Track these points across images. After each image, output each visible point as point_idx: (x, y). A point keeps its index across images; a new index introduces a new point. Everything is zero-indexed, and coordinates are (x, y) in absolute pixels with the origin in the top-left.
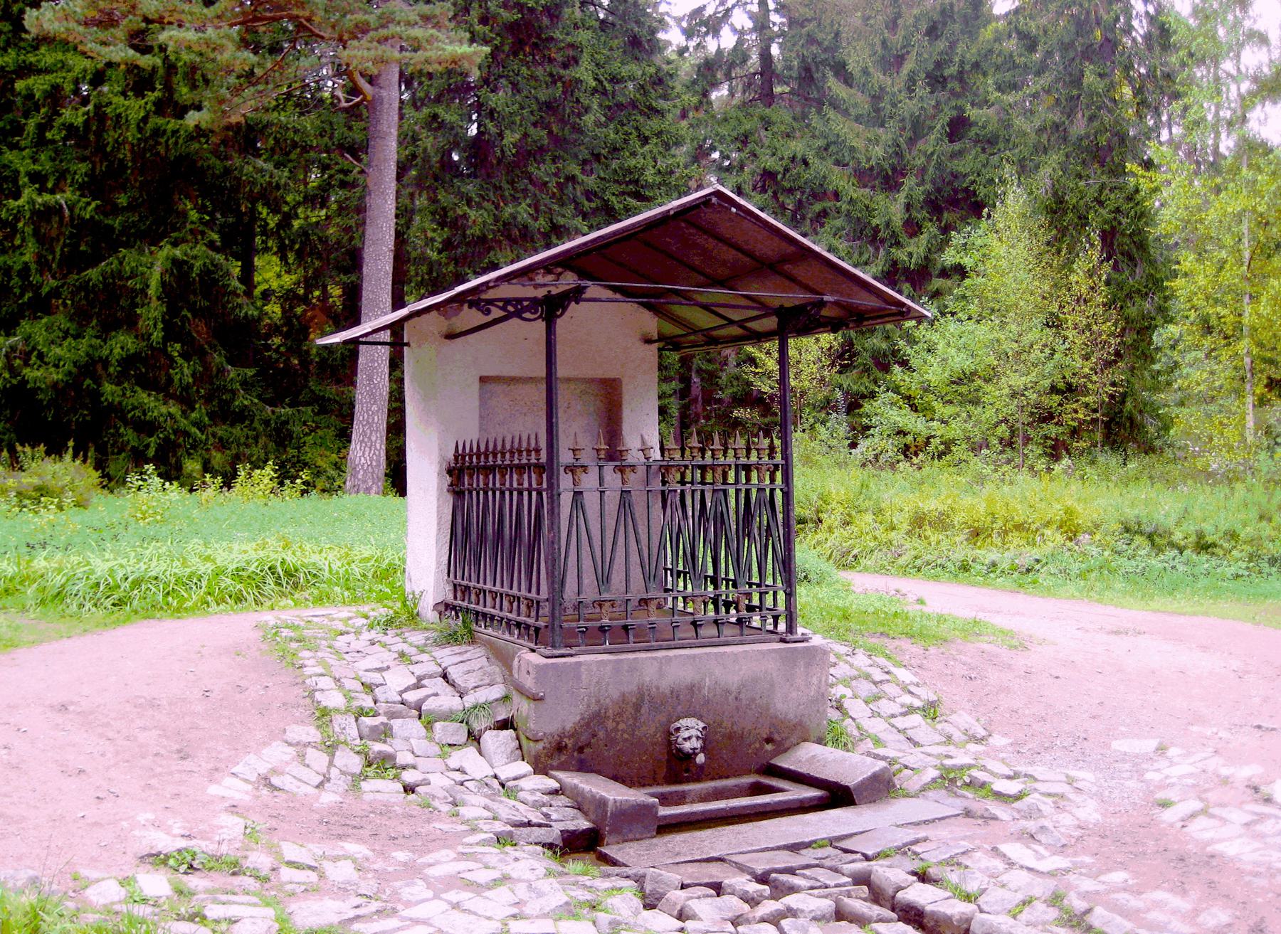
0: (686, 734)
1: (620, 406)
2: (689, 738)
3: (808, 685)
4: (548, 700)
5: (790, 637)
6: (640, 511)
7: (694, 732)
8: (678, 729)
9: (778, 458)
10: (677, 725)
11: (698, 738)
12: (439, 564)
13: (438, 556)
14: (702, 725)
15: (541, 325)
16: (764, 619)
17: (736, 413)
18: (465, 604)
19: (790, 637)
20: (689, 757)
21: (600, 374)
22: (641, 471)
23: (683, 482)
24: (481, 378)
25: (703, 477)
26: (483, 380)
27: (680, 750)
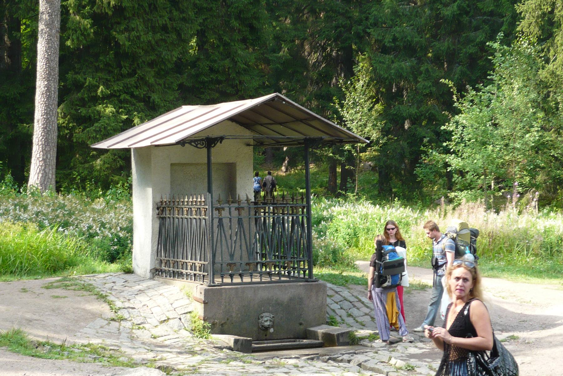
0: (266, 319)
1: (235, 174)
2: (267, 321)
5: (309, 280)
6: (246, 225)
8: (262, 317)
9: (305, 203)
10: (262, 315)
12: (152, 251)
13: (152, 247)
15: (205, 150)
16: (299, 272)
17: (487, 44)
18: (167, 269)
19: (309, 280)
20: (267, 329)
21: (225, 161)
22: (246, 209)
23: (283, 214)
24: (172, 165)
25: (293, 212)
26: (172, 165)
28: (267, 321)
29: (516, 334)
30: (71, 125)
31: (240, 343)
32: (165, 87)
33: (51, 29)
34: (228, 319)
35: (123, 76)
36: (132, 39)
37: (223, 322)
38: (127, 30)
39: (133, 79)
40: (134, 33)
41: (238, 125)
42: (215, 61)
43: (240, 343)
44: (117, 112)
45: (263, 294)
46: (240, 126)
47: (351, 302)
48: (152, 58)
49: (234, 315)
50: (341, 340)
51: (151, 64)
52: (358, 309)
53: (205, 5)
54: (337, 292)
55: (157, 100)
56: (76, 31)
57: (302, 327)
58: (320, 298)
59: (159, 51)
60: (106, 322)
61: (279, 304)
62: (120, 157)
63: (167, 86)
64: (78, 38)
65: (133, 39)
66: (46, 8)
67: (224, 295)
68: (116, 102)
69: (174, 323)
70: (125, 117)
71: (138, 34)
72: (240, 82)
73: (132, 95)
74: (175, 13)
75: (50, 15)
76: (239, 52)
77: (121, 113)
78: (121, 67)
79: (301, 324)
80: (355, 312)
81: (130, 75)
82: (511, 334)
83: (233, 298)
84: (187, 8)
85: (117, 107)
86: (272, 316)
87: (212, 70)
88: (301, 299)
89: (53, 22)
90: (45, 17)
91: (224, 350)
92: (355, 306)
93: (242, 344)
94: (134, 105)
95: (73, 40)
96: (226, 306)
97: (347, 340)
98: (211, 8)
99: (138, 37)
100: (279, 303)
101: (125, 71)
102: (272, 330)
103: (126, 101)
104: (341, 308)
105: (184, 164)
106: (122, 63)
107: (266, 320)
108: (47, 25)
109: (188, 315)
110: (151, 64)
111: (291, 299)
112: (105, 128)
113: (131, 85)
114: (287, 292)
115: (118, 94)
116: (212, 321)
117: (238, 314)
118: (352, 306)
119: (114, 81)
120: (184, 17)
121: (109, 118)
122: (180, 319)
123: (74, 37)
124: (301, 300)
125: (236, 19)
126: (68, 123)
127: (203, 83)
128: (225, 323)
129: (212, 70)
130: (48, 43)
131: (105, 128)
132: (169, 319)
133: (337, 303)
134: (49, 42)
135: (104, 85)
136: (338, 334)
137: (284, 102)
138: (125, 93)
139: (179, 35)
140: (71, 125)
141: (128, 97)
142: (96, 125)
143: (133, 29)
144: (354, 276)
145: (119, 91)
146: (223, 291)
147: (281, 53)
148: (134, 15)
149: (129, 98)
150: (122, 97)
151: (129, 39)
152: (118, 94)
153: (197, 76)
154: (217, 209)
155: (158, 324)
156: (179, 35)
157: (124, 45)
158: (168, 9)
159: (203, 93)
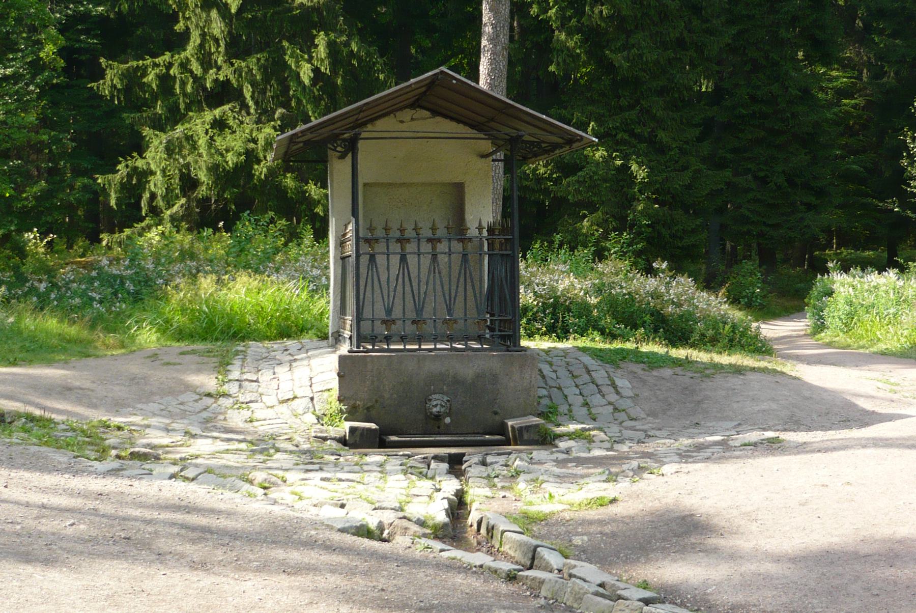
0: (435, 403)
2: (436, 405)
7: (439, 402)
8: (430, 400)
11: (442, 406)
20: (438, 417)
27: (431, 413)
28: (436, 405)
29: (783, 436)
30: (555, 176)
31: (358, 433)
32: (682, 123)
33: (495, 46)
34: (377, 401)
35: (622, 109)
36: (631, 58)
37: (369, 404)
38: (625, 47)
39: (632, 112)
40: (634, 51)
43: (358, 433)
44: (610, 156)
45: (431, 367)
48: (661, 83)
49: (387, 395)
50: (526, 437)
51: (661, 92)
53: (744, 12)
55: (665, 140)
56: (563, 51)
57: (497, 418)
58: (527, 376)
59: (672, 74)
60: (198, 397)
62: (613, 216)
63: (684, 121)
64: (564, 61)
65: (634, 59)
66: (490, 18)
67: (369, 367)
68: (610, 143)
69: (300, 405)
70: (619, 163)
71: (640, 52)
72: (793, 114)
73: (632, 134)
74: (696, 22)
75: (494, 27)
77: (615, 158)
78: (619, 97)
79: (496, 413)
80: (597, 399)
81: (631, 107)
82: (770, 434)
85: (611, 150)
86: (446, 398)
87: (753, 98)
89: (498, 36)
90: (488, 29)
91: (328, 442)
93: (362, 435)
94: (635, 146)
95: (558, 64)
96: (373, 382)
97: (536, 438)
98: (754, 16)
99: (641, 56)
100: (457, 381)
101: (624, 102)
102: (448, 420)
103: (623, 142)
105: (390, 184)
106: (620, 91)
107: (437, 404)
108: (490, 40)
109: (326, 394)
110: (661, 92)
111: (478, 376)
112: (591, 177)
113: (631, 120)
114: (471, 365)
115: (614, 133)
116: (352, 402)
119: (610, 116)
121: (598, 163)
122: (312, 399)
123: (560, 60)
124: (495, 378)
126: (551, 174)
128: (372, 406)
129: (753, 98)
130: (491, 64)
131: (591, 177)
132: (295, 397)
134: (492, 62)
135: (596, 121)
136: (521, 427)
137: (454, 82)
138: (625, 131)
140: (555, 176)
141: (626, 136)
142: (580, 173)
143: (633, 46)
144: (650, 352)
145: (616, 128)
147: (885, 79)
148: (636, 27)
149: (627, 138)
150: (619, 136)
151: (627, 59)
152: (614, 133)
154: (367, 241)
155: (276, 403)
157: (620, 66)
158: (686, 19)
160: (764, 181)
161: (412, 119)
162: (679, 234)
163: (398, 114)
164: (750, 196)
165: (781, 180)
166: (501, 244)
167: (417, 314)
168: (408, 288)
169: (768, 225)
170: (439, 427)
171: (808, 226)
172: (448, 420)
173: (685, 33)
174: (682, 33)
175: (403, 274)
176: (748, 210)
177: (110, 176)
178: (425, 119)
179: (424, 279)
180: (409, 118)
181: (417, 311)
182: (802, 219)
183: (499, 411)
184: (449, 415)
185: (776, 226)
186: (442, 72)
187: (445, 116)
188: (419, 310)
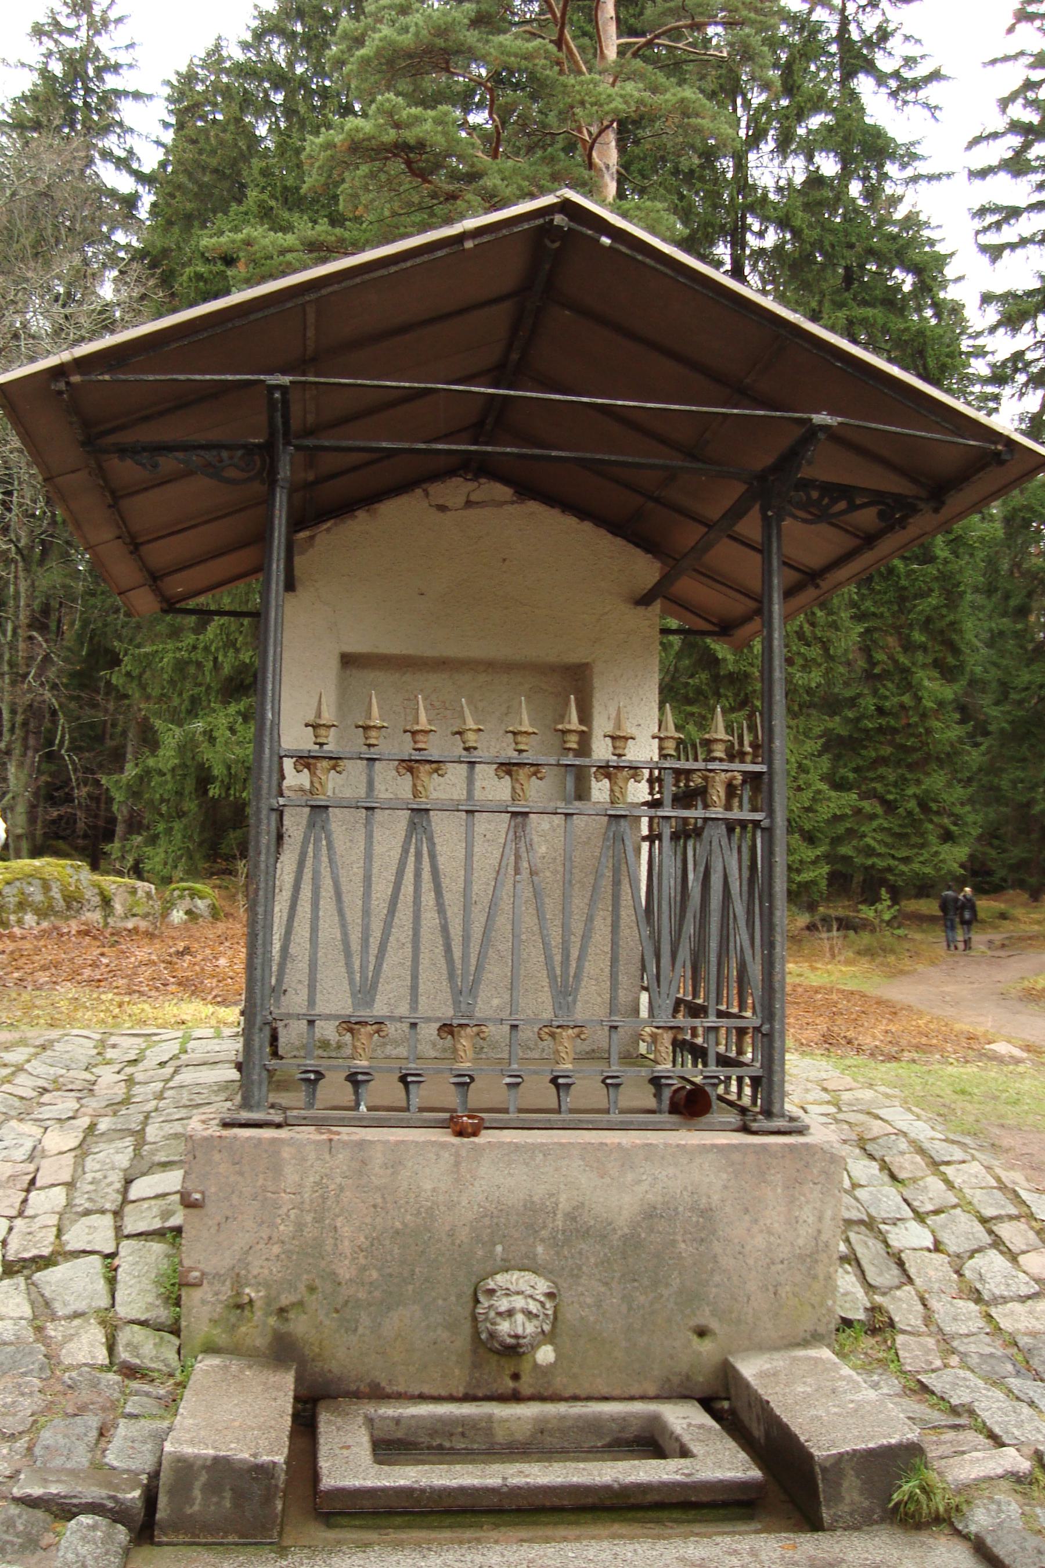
0: (503, 1305)
2: (510, 1313)
3: (793, 1222)
4: (211, 1207)
7: (519, 1302)
10: (491, 1285)
11: (529, 1314)
14: (543, 1286)
20: (513, 1350)
26: (348, 661)
27: (492, 1335)
41: (603, 532)
42: (886, 698)
46: (610, 536)
47: (984, 1221)
49: (345, 1271)
52: (1013, 1257)
53: (872, 609)
54: (935, 1165)
57: (706, 1347)
58: (807, 1214)
61: (585, 1233)
67: (291, 1176)
76: (926, 683)
83: (341, 1188)
84: (839, 608)
88: (706, 1213)
92: (998, 1243)
96: (300, 1226)
104: (937, 1247)
111: (650, 1214)
114: (630, 1177)
117: (364, 1269)
118: (988, 1239)
120: (834, 621)
125: (921, 631)
127: (867, 731)
129: (880, 711)
133: (920, 1217)
137: (606, 241)
139: (826, 650)
146: (286, 1153)
153: (858, 720)
156: (826, 650)
159: (865, 747)
160: (890, 807)
161: (469, 504)
162: (795, 866)
163: (434, 488)
164: (875, 824)
165: (912, 804)
166: (731, 790)
167: (456, 1003)
168: (430, 918)
169: (899, 859)
170: (516, 1377)
171: (943, 861)
172: (545, 1355)
173: (806, 626)
174: (801, 627)
175: (418, 875)
176: (874, 839)
177: (116, 777)
178: (501, 504)
179: (481, 887)
180: (461, 500)
181: (457, 993)
182: (937, 853)
183: (714, 1324)
184: (547, 1338)
185: (906, 860)
186: (567, 207)
187: (550, 499)
188: (464, 986)
